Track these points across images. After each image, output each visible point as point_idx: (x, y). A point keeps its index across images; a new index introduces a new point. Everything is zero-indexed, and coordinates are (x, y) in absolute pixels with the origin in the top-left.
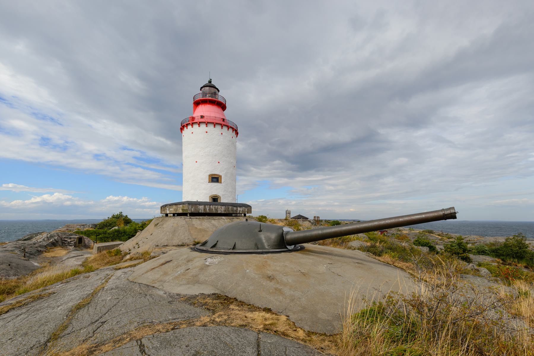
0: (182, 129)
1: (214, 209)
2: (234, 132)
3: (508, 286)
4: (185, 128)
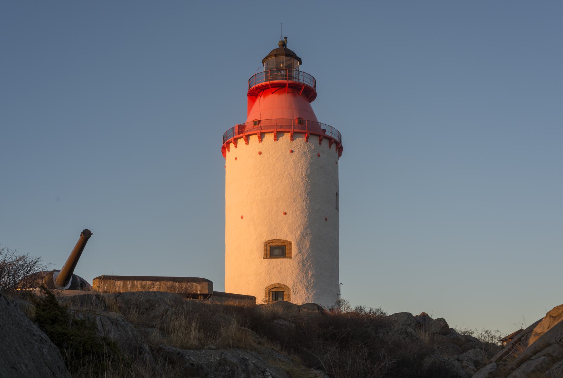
0: (225, 148)
2: (334, 146)
3: (72, 373)
4: (232, 145)
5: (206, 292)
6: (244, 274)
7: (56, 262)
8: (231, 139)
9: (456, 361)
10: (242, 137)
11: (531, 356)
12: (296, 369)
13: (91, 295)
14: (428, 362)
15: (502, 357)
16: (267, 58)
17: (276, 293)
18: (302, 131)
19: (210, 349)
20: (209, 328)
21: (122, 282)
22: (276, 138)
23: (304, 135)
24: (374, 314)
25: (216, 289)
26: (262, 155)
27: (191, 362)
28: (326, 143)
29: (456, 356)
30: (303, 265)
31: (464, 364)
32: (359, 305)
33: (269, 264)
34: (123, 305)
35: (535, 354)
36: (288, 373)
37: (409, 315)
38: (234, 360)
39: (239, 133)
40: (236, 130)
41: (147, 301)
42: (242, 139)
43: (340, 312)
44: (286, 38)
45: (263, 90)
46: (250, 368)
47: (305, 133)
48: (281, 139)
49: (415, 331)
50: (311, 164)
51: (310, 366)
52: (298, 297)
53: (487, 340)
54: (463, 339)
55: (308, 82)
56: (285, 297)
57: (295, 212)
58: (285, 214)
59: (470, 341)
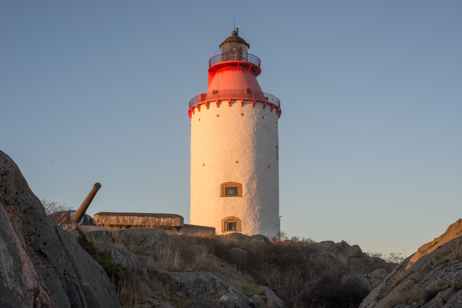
0: (191, 111)
1: (128, 220)
2: (274, 110)
4: (196, 109)
5: (179, 225)
6: (206, 210)
7: (76, 206)
8: (196, 105)
9: (366, 279)
10: (204, 103)
11: (403, 279)
12: (249, 285)
13: (103, 232)
14: (345, 279)
15: (389, 278)
16: (223, 44)
17: (230, 224)
18: (250, 99)
19: (188, 271)
20: (187, 257)
21: (115, 217)
22: (230, 104)
23: (251, 102)
24: (306, 242)
25: (185, 222)
26: (219, 117)
27: (176, 281)
28: (268, 108)
29: (366, 275)
30: (251, 202)
31: (371, 281)
32: (295, 236)
33: (225, 201)
34: (126, 239)
35: (406, 278)
36: (244, 288)
37: (332, 243)
38: (206, 280)
39: (202, 100)
40: (200, 98)
41: (142, 236)
42: (204, 105)
43: (281, 242)
44: (237, 29)
45: (220, 67)
46: (217, 285)
47: (253, 101)
48: (234, 105)
49: (336, 255)
50: (257, 124)
51: (259, 283)
52: (248, 229)
53: (392, 260)
54: (373, 260)
55: (254, 62)
56: (237, 227)
57: (245, 161)
58: (237, 162)
59: (378, 262)
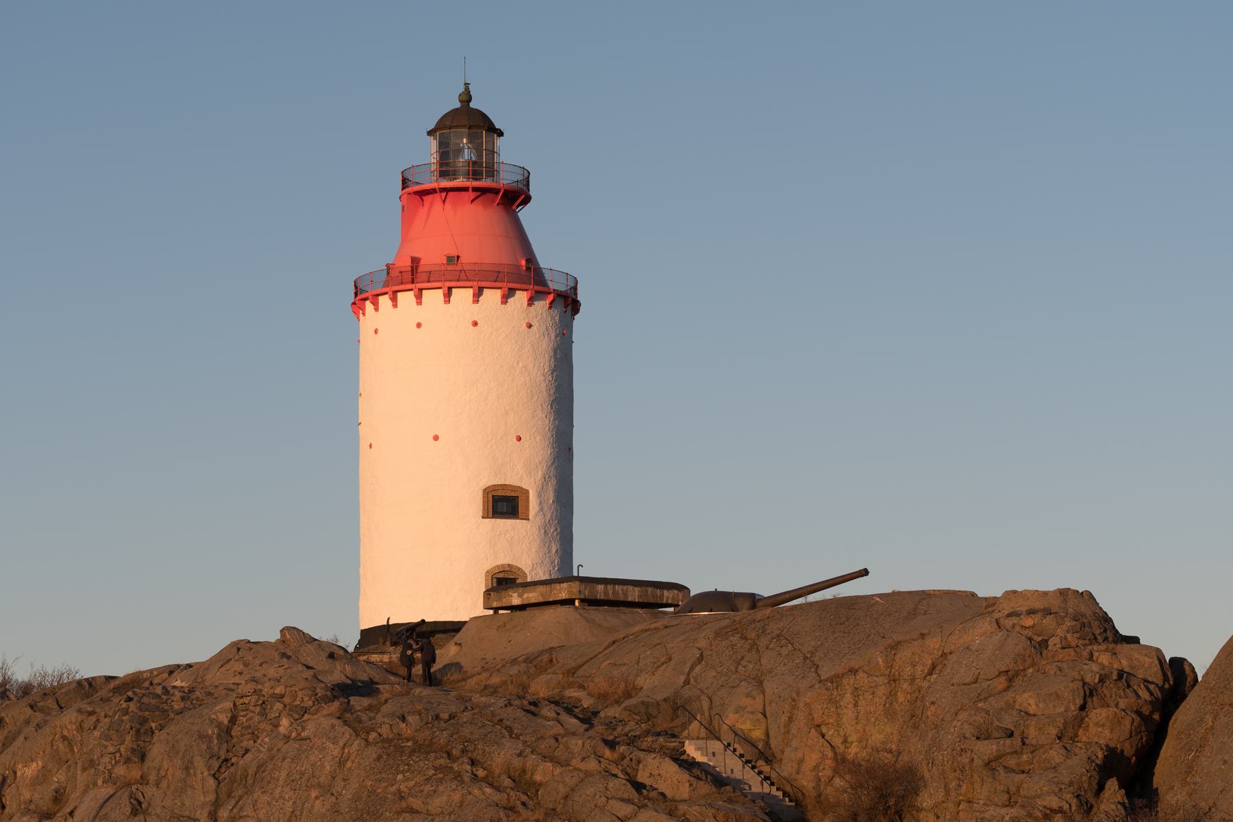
4: (369, 305)
48: (511, 300)
58: (519, 439)
